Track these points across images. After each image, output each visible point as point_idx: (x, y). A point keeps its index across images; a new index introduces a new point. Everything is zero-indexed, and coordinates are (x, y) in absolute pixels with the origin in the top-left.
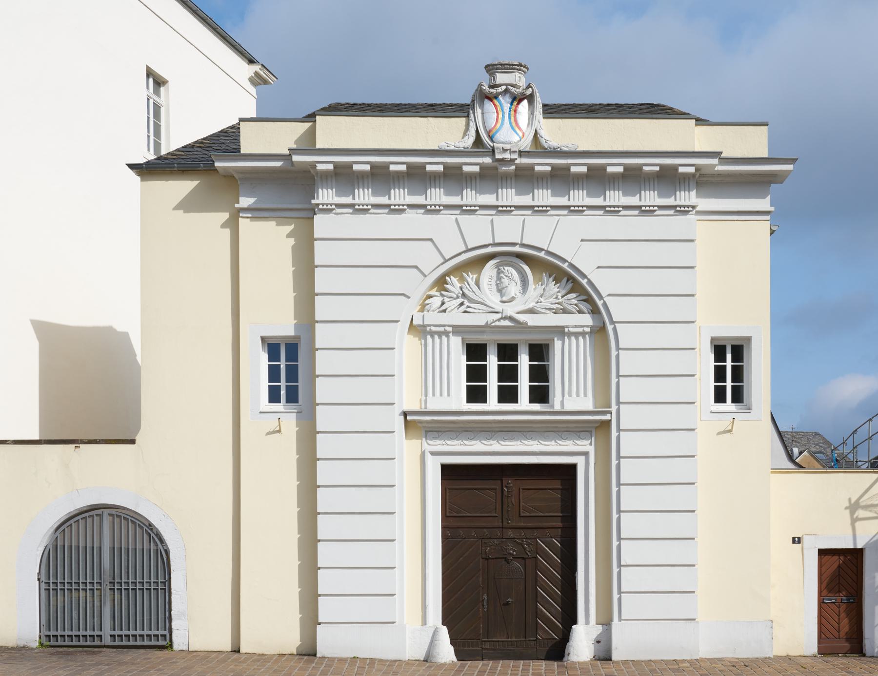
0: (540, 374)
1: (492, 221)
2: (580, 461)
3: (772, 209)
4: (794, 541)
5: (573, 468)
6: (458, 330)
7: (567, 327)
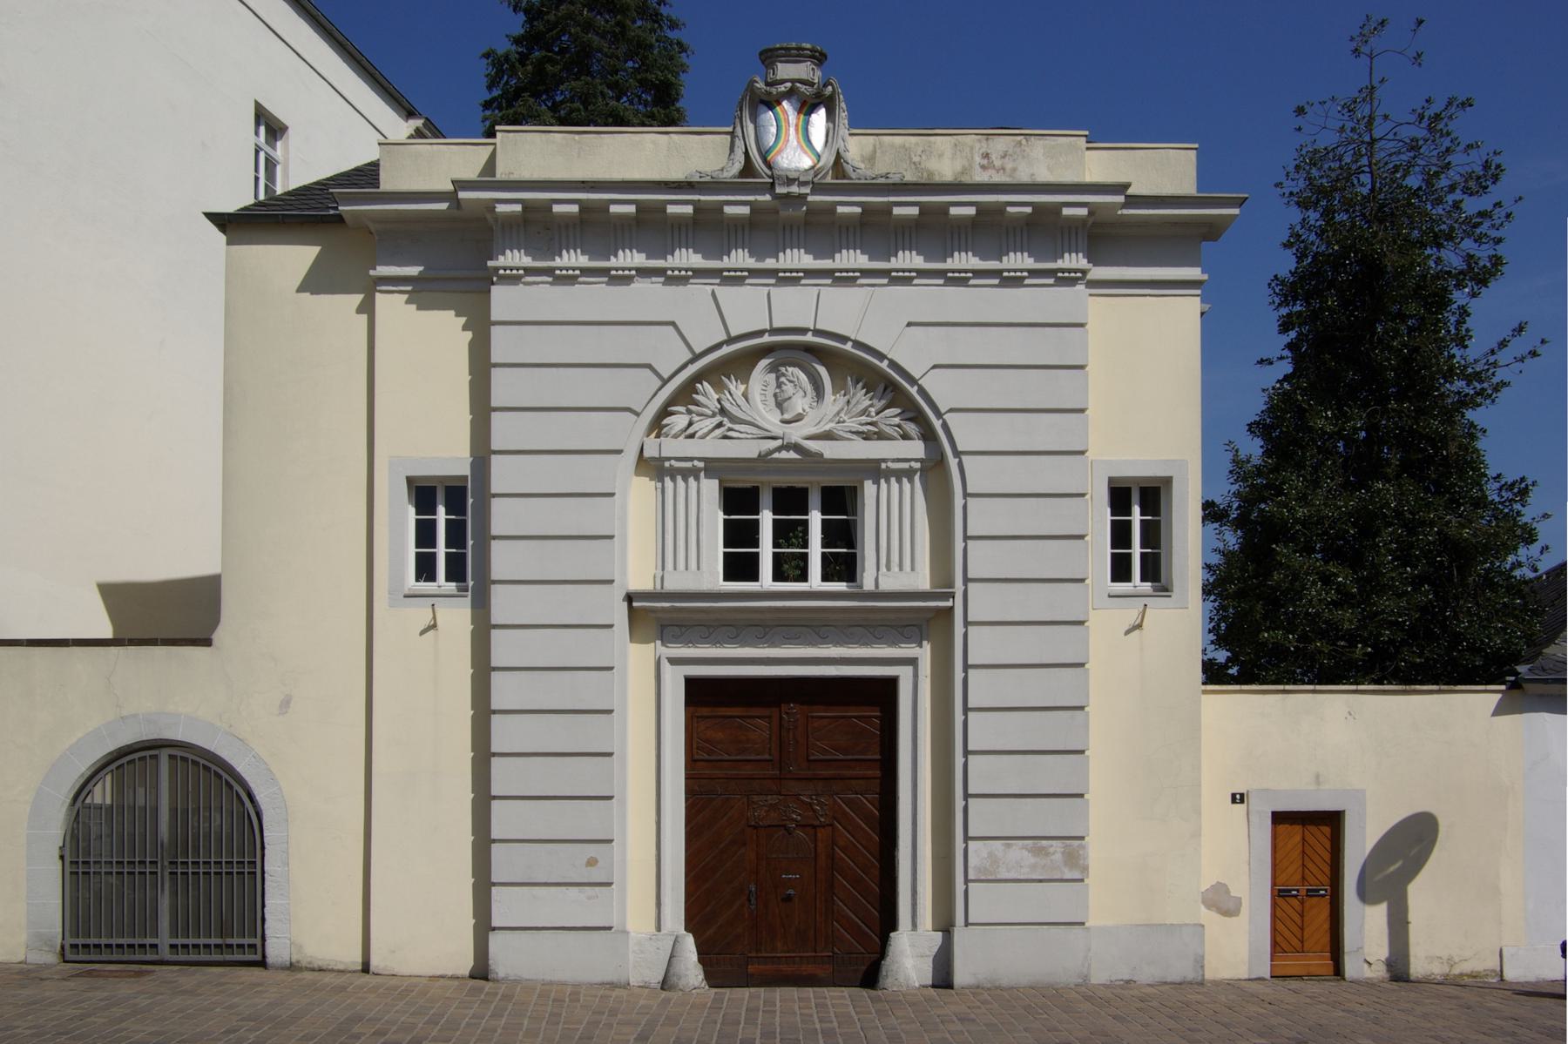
0: (842, 535)
1: (820, 290)
2: (904, 674)
3: (1205, 277)
4: (1234, 800)
5: (891, 684)
6: (713, 467)
7: (885, 460)
